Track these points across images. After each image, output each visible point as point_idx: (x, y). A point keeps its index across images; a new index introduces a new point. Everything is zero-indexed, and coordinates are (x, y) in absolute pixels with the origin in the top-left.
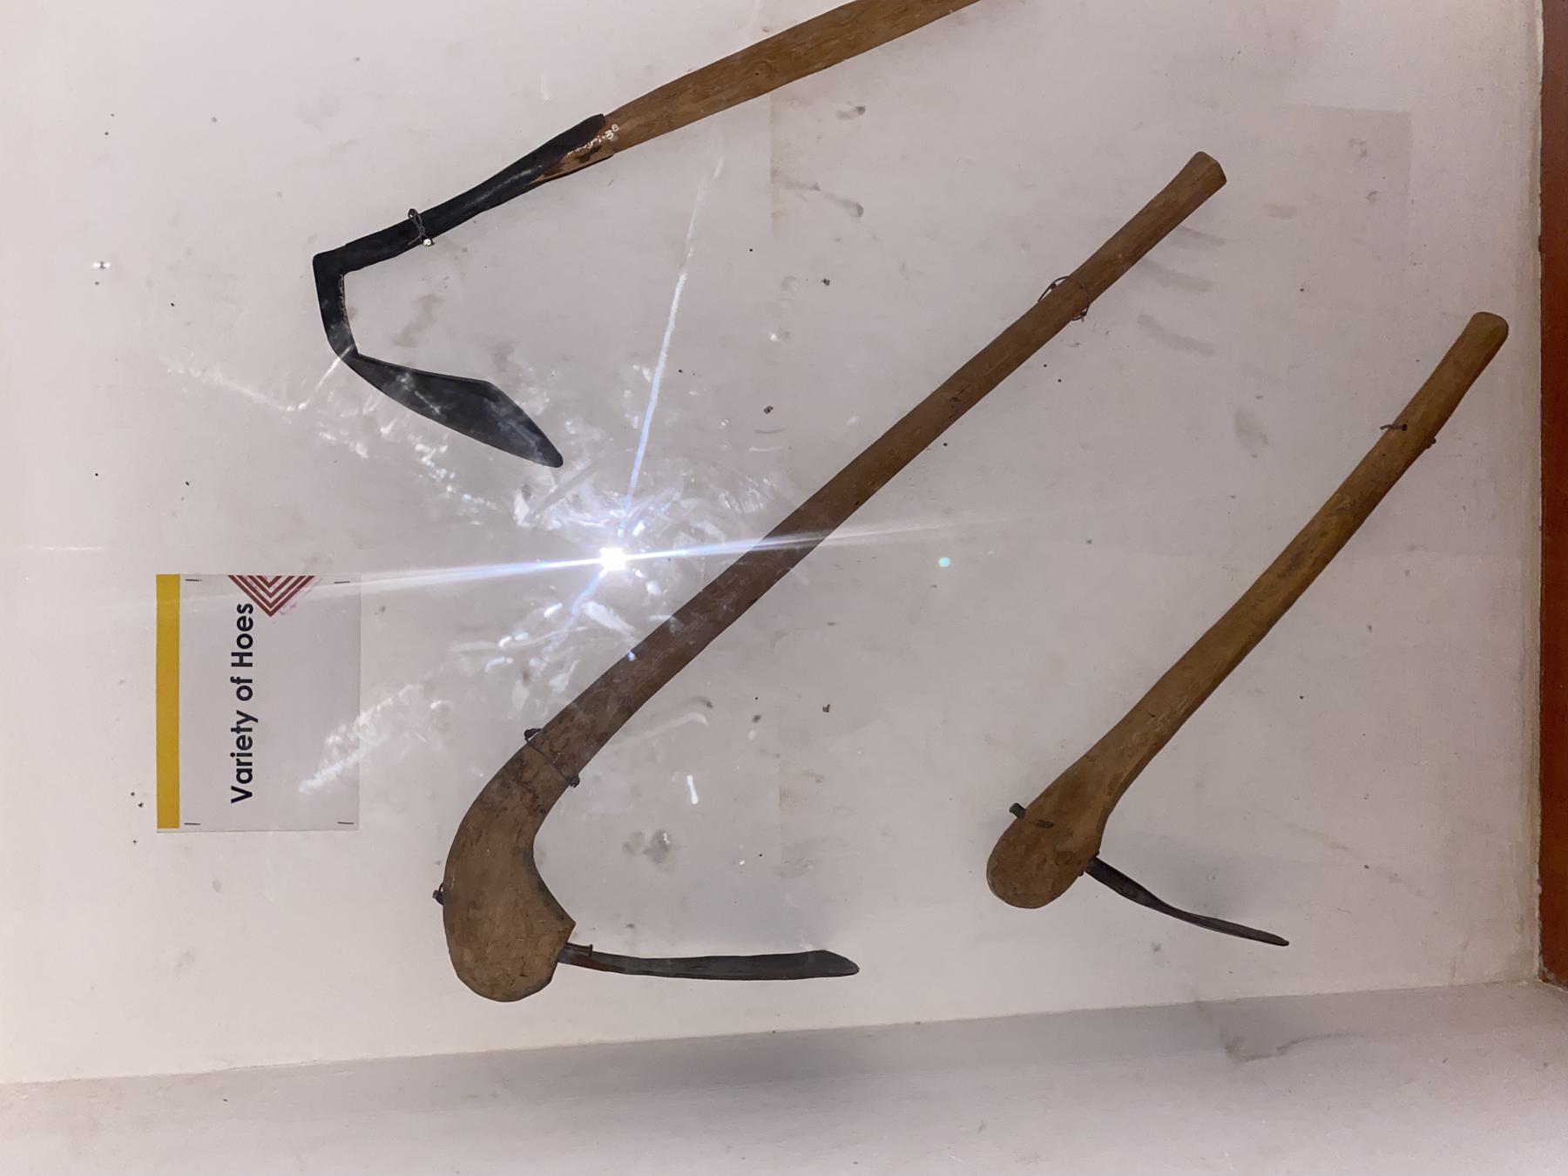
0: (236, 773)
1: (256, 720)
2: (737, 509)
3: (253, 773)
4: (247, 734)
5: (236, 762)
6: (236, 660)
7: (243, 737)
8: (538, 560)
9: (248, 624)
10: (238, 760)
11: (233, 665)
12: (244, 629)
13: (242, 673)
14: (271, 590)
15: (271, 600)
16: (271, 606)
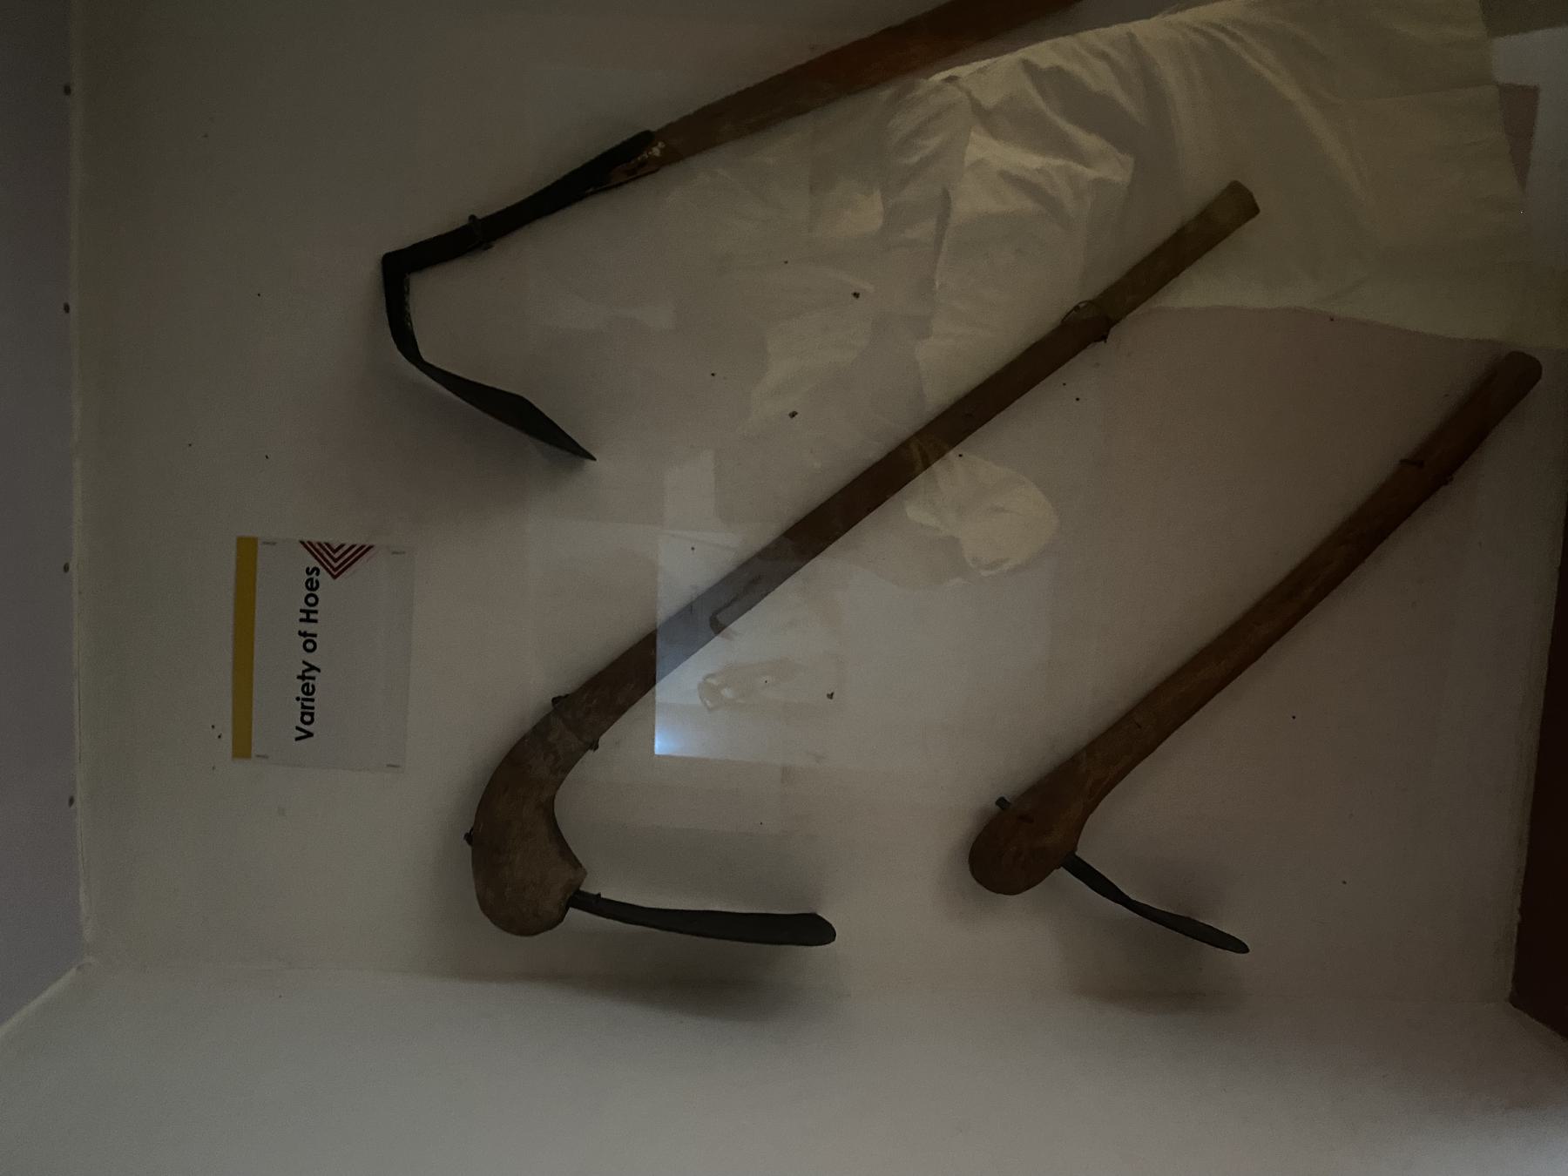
1: (319, 670)
3: (315, 717)
4: (311, 682)
5: (300, 706)
6: (304, 616)
7: (307, 684)
9: (315, 585)
10: (302, 704)
11: (301, 620)
12: (311, 589)
13: (309, 628)
14: (336, 556)
15: (335, 565)
16: (335, 570)
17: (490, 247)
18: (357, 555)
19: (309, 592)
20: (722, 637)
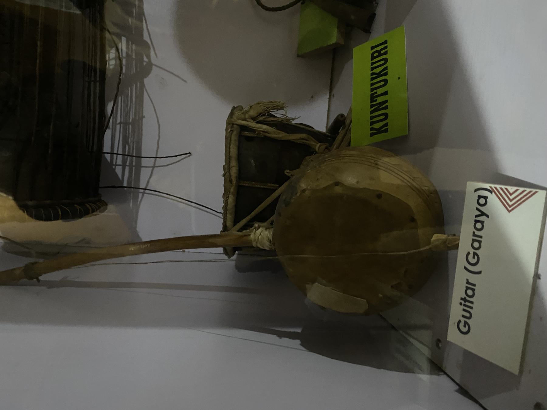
0: (477, 198)
1: (488, 216)
2: (342, 156)
8: (375, 13)
10: (474, 232)
14: (511, 197)
15: (510, 203)
16: (510, 207)
17: (105, 79)
18: (520, 202)
19: (477, 252)
20: (141, 239)
